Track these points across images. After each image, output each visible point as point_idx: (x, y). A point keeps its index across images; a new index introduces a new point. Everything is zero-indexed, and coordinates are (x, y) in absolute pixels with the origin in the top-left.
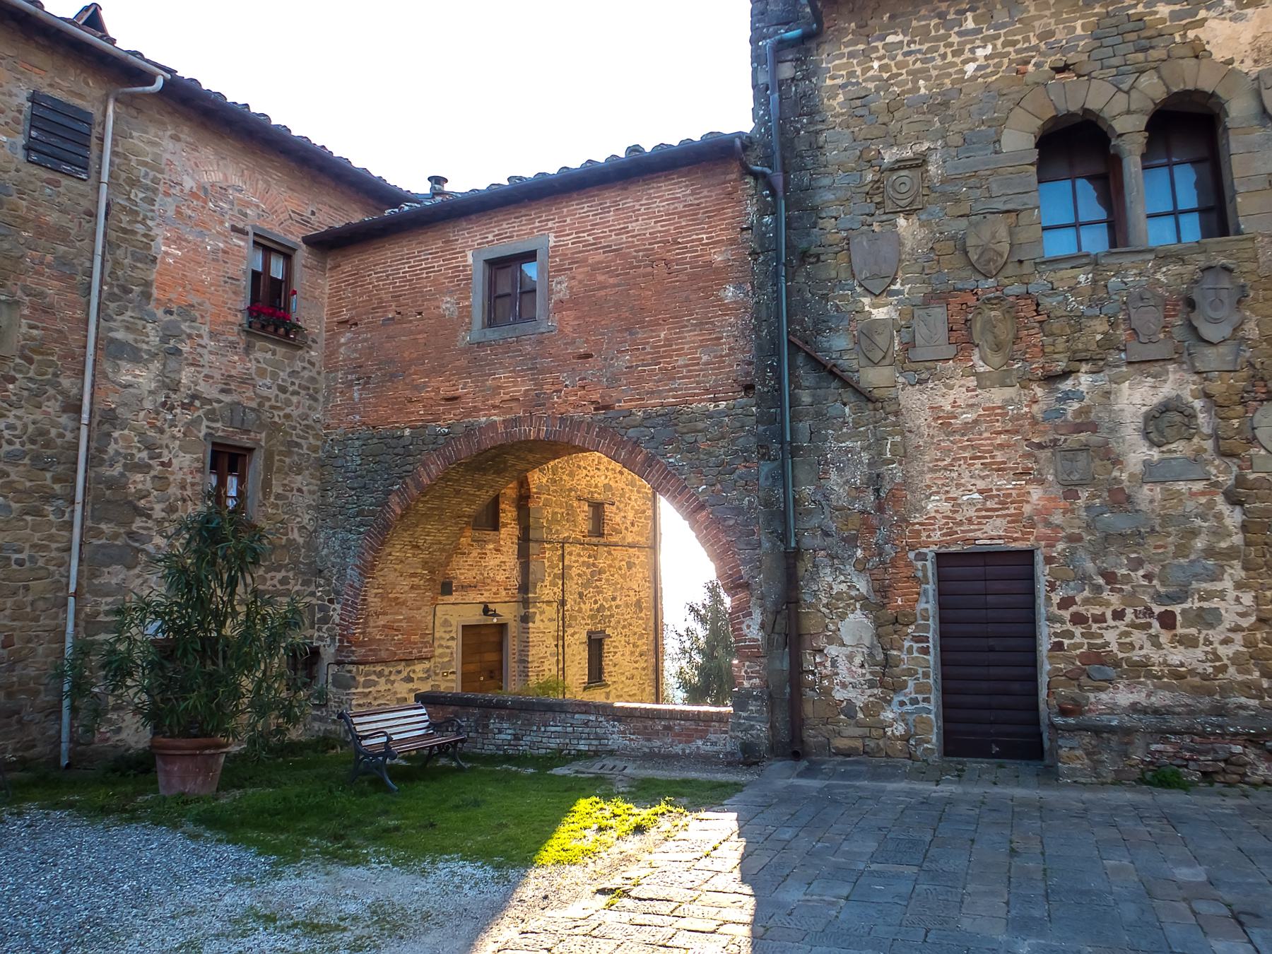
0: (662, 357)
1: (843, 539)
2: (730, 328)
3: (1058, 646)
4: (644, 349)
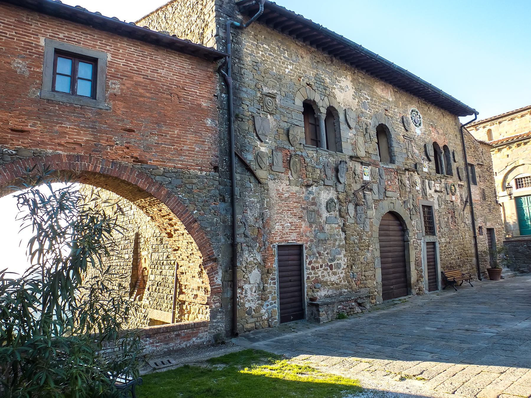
0: (176, 143)
1: (252, 239)
2: (209, 138)
3: (308, 278)
4: (166, 136)
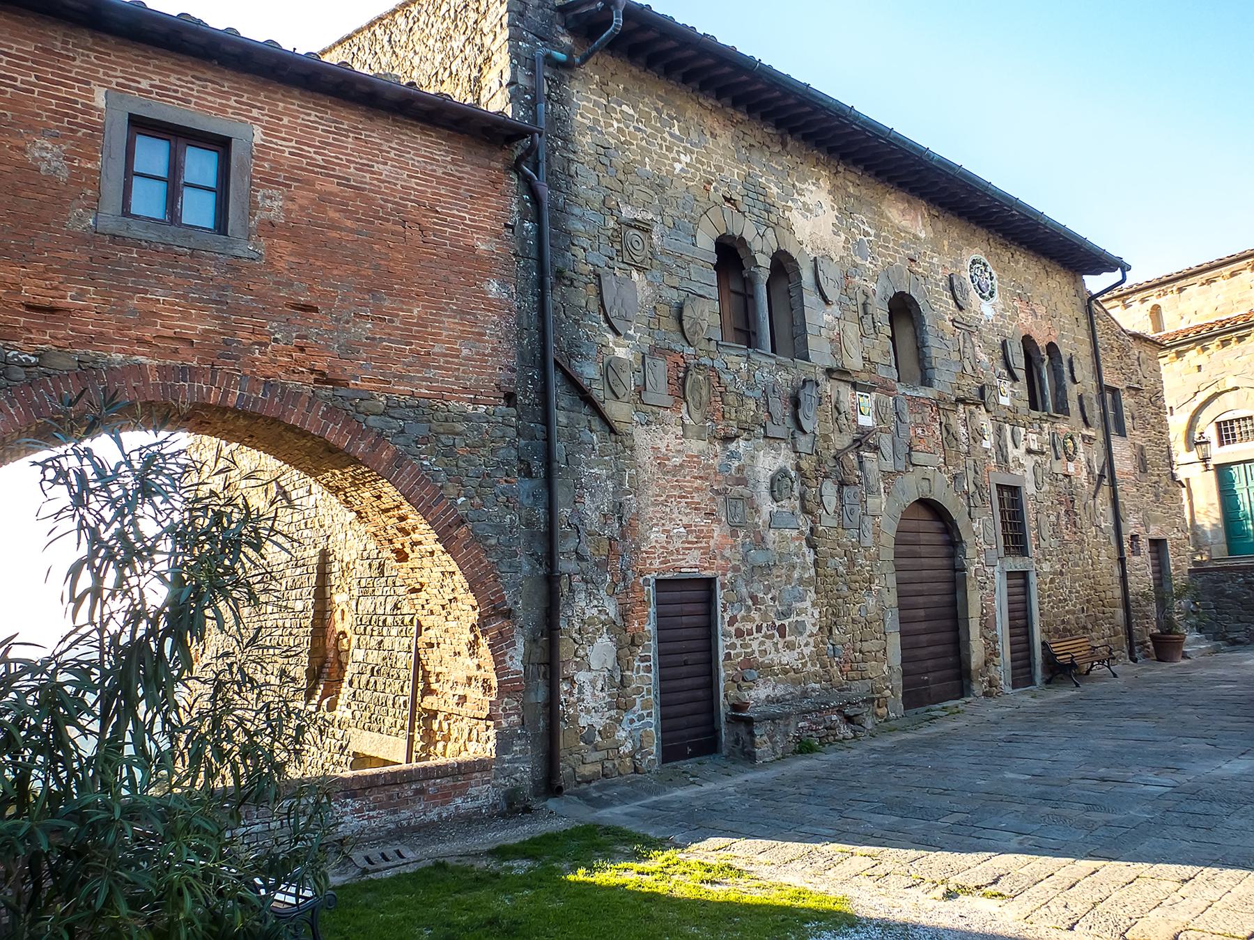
0: (415, 337)
1: (596, 564)
2: (493, 326)
3: (728, 656)
4: (391, 321)
